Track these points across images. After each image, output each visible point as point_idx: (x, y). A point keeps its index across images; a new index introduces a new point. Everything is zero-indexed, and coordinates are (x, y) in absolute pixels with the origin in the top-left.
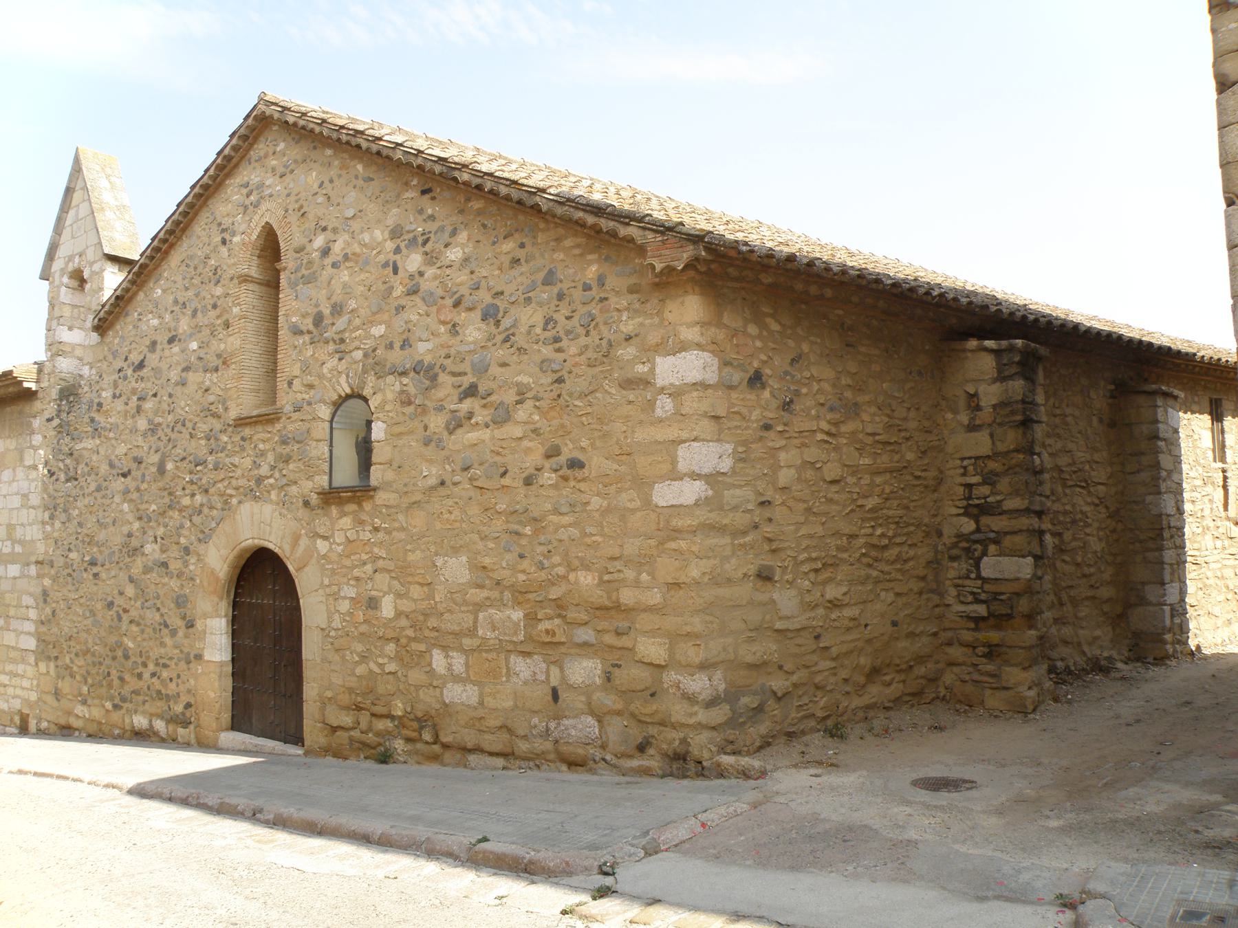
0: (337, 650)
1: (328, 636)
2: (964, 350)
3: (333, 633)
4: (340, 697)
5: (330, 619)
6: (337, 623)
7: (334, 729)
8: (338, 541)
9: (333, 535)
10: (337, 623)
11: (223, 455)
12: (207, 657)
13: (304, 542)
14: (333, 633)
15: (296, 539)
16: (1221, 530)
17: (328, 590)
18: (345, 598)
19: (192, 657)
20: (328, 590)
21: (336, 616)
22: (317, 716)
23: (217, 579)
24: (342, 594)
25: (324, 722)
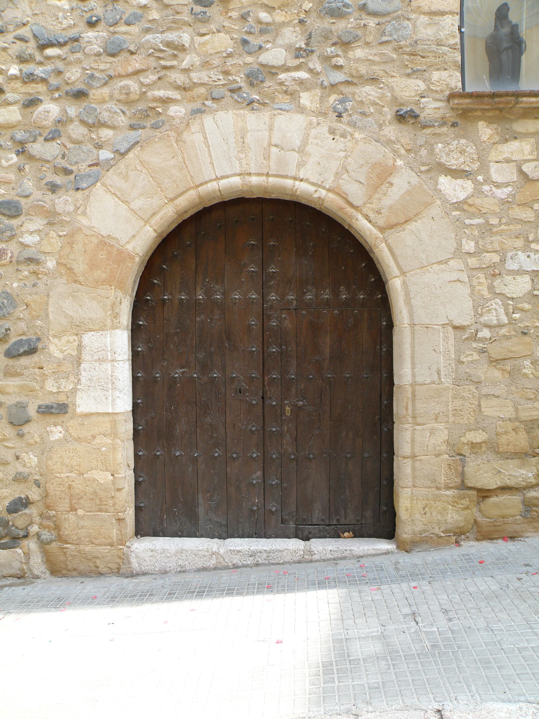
0: (494, 362)
1: (474, 337)
2: (414, 385)
3: (485, 333)
4: (503, 439)
5: (479, 306)
6: (496, 313)
7: (484, 494)
8: (496, 177)
9: (484, 168)
10: (496, 313)
11: (134, 29)
12: (84, 404)
13: (403, 181)
14: (485, 333)
15: (382, 176)
16: (55, 484)
17: (473, 262)
18: (520, 272)
19: (32, 410)
20: (473, 262)
21: (496, 304)
22: (442, 479)
23: (121, 256)
24: (512, 265)
25: (463, 486)
